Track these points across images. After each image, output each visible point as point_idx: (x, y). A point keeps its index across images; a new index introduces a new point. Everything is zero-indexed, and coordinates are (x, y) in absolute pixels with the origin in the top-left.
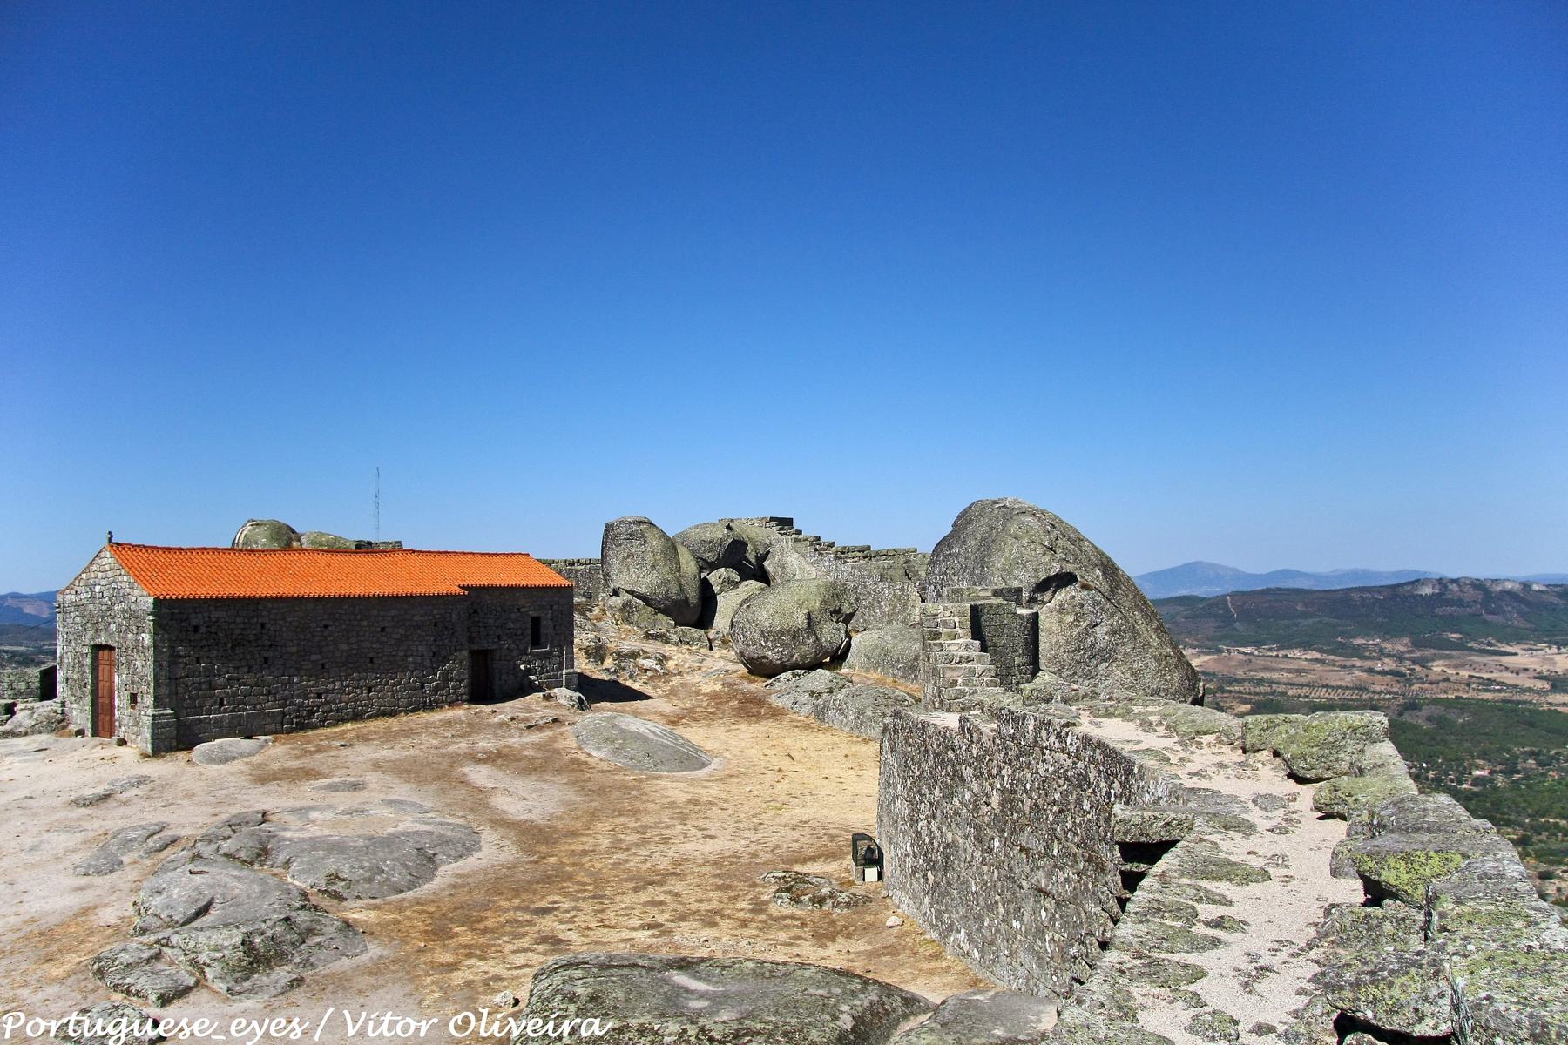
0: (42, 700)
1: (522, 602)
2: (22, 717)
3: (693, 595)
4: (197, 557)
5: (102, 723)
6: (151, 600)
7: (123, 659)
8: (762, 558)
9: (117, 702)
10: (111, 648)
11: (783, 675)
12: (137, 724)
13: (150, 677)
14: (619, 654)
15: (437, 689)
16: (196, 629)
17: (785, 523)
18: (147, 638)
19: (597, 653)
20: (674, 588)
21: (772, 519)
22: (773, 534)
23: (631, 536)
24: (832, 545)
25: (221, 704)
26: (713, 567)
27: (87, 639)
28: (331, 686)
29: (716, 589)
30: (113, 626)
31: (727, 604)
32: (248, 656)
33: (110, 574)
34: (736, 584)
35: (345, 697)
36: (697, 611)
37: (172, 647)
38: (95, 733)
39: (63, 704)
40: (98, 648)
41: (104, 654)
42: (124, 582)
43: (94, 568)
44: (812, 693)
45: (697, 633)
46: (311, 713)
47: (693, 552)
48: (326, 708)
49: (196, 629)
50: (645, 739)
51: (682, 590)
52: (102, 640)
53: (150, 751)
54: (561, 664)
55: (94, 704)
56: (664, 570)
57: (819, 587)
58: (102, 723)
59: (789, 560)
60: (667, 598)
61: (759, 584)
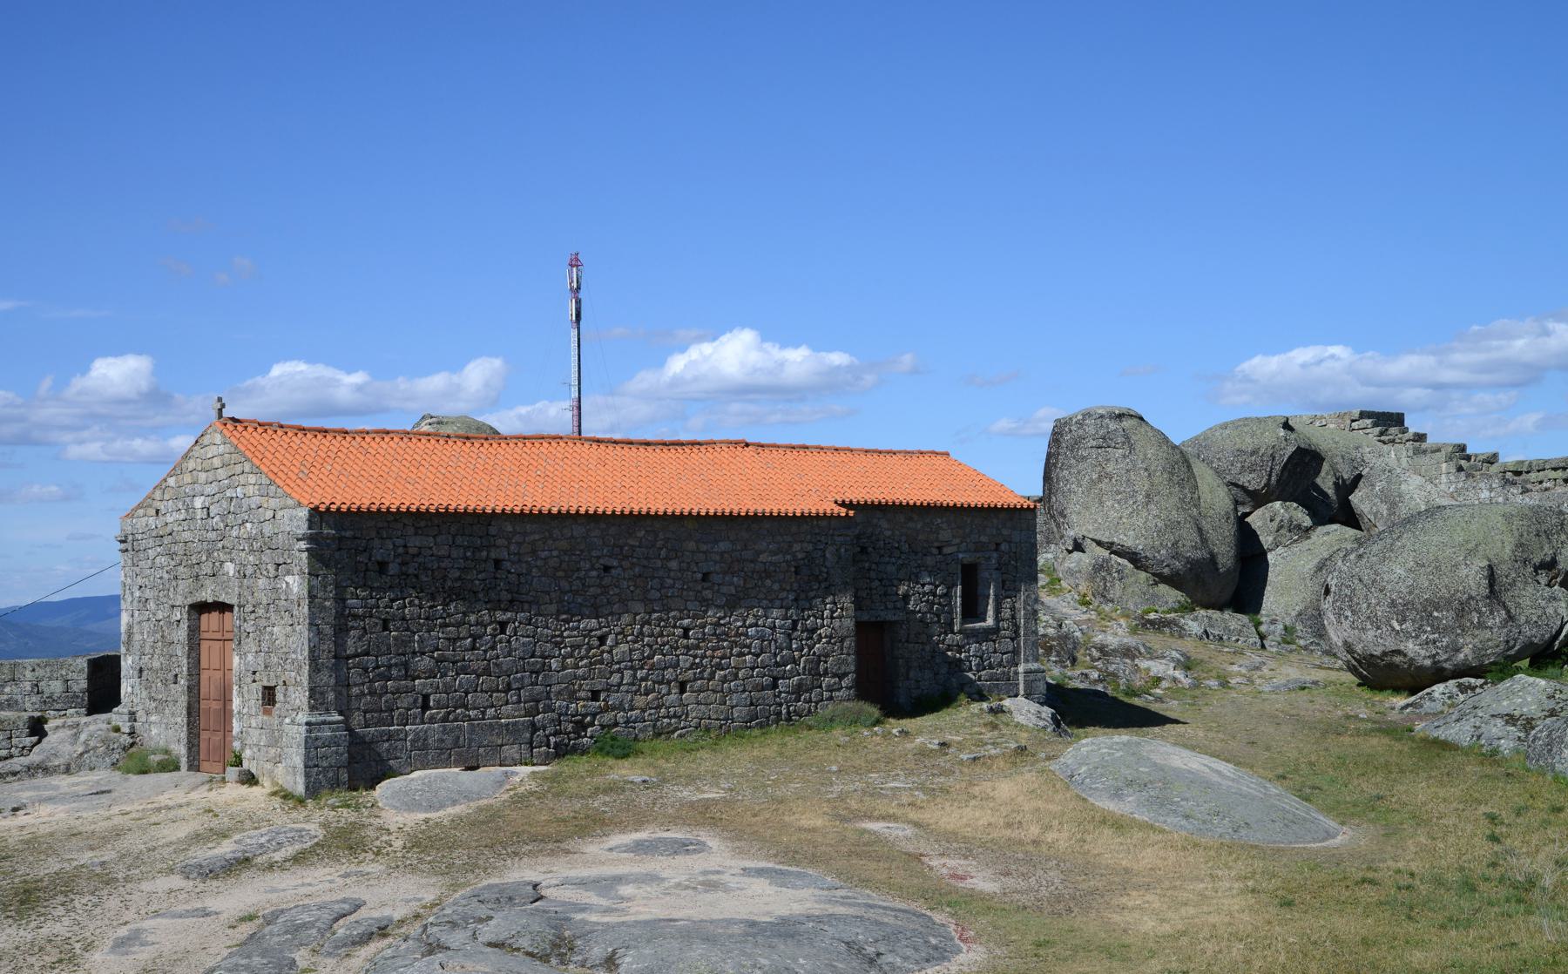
0: (89, 714)
1: (945, 535)
2: (57, 739)
3: (1225, 550)
4: (374, 446)
5: (207, 745)
6: (303, 513)
7: (249, 627)
8: (1347, 487)
9: (236, 703)
10: (224, 608)
11: (1438, 689)
12: (274, 742)
13: (303, 655)
14: (1102, 649)
15: (798, 691)
16: (382, 567)
17: (1388, 421)
18: (295, 584)
19: (1067, 649)
20: (1189, 537)
21: (1363, 415)
22: (1367, 439)
23: (1106, 442)
24: (1492, 459)
25: (425, 707)
26: (1259, 499)
27: (182, 596)
28: (615, 679)
29: (1266, 540)
30: (230, 568)
31: (1291, 571)
32: (465, 620)
33: (222, 473)
34: (1306, 532)
35: (640, 701)
36: (1236, 582)
37: (340, 599)
38: (194, 766)
39: (132, 716)
40: (201, 608)
41: (210, 621)
42: (249, 488)
43: (191, 465)
44: (1511, 719)
45: (1234, 621)
46: (581, 727)
47: (1218, 472)
48: (607, 718)
49: (382, 567)
50: (1207, 785)
51: (1204, 540)
52: (207, 596)
53: (300, 789)
54: (1016, 652)
55: (193, 711)
56: (1168, 505)
57: (1508, 518)
58: (207, 745)
59: (1400, 482)
60: (1176, 556)
61: (1350, 532)
